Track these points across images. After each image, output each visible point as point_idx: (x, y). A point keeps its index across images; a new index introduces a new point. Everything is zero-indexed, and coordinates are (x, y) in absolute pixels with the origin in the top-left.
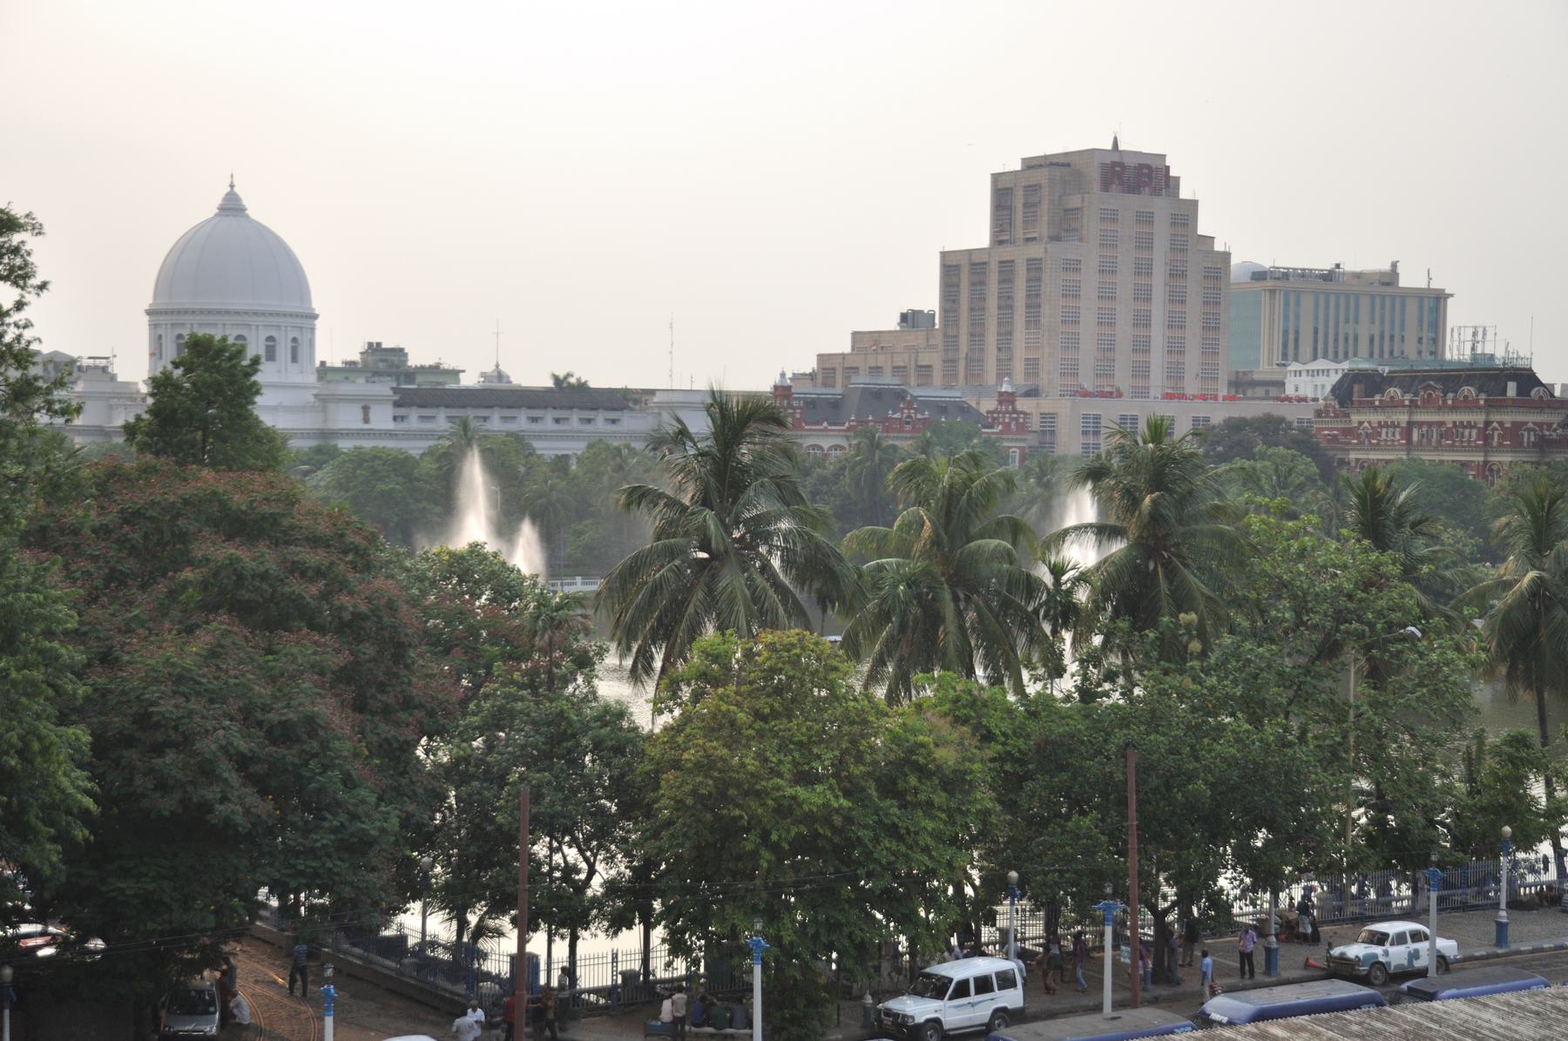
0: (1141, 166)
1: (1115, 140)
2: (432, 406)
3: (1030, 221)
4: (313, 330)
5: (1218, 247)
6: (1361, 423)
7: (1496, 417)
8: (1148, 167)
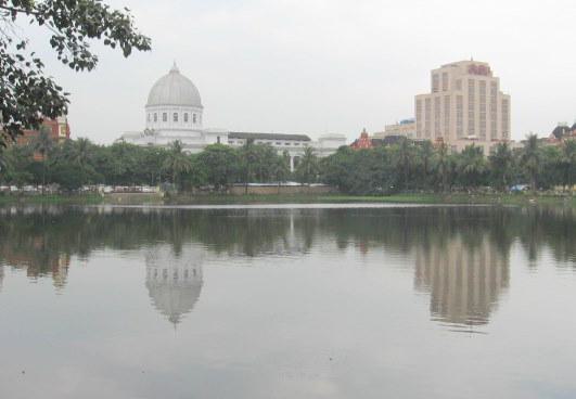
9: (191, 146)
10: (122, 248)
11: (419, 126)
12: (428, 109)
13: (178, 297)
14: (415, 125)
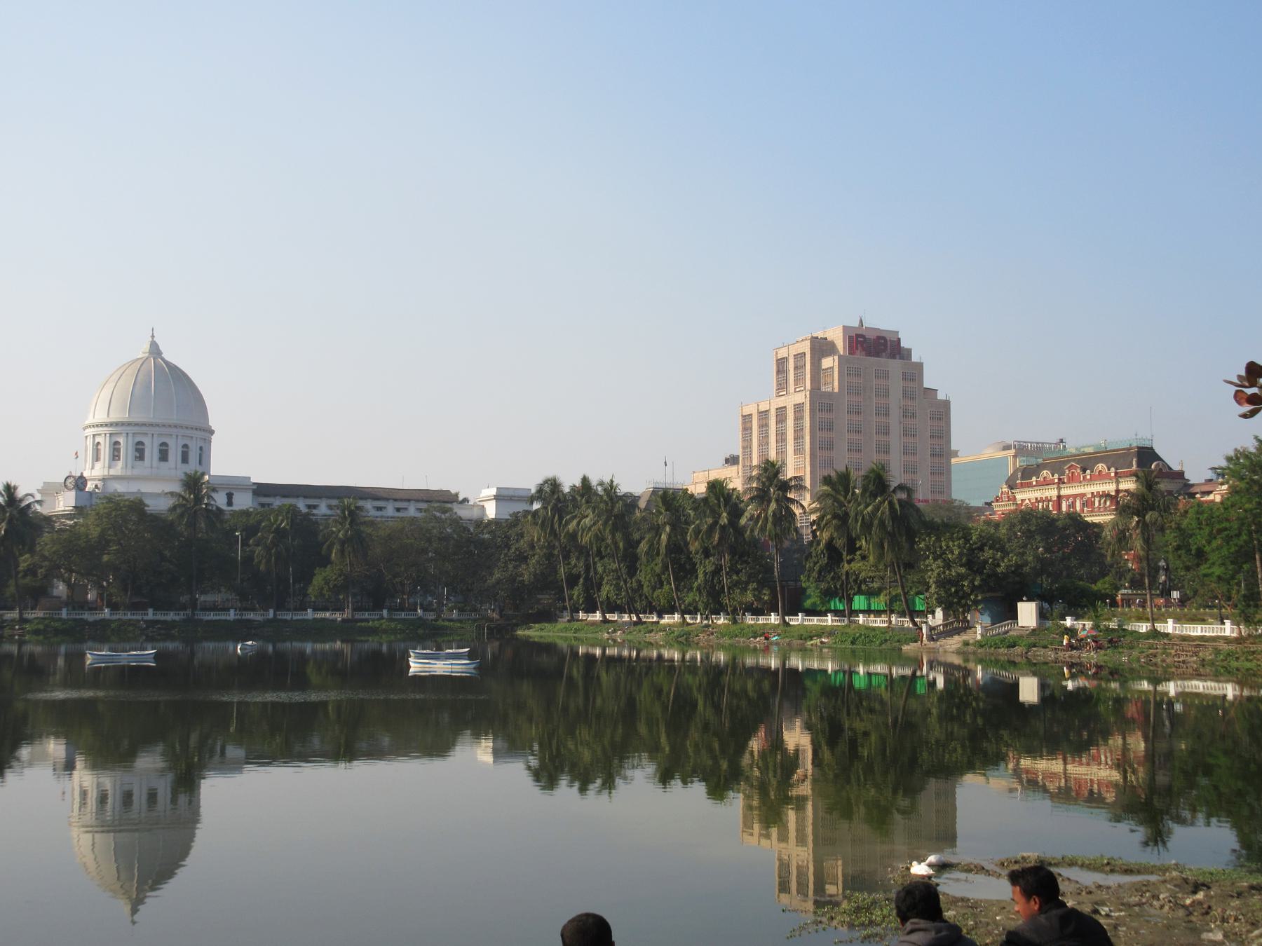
0: (879, 338)
2: (315, 497)
3: (799, 379)
5: (941, 396)
6: (1023, 500)
8: (884, 338)
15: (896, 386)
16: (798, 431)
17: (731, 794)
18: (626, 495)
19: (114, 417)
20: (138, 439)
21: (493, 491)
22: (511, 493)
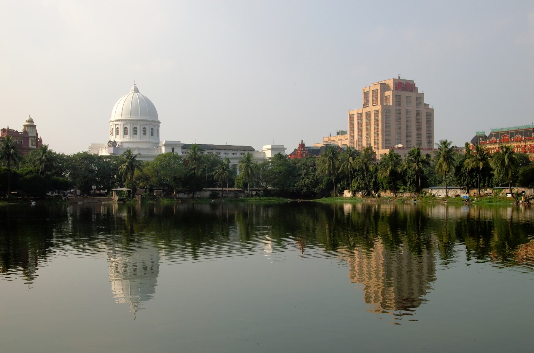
1: (399, 77)
4: (159, 126)
7: (528, 143)
8: (409, 84)
9: (145, 156)
10: (407, 83)
11: (352, 137)
12: (360, 124)
13: (143, 278)
14: (348, 136)
15: (414, 101)
16: (376, 122)
17: (93, 154)
18: (299, 147)
19: (124, 118)
20: (135, 126)
21: (270, 146)
22: (277, 147)
